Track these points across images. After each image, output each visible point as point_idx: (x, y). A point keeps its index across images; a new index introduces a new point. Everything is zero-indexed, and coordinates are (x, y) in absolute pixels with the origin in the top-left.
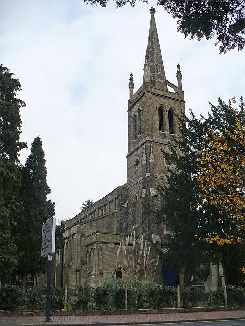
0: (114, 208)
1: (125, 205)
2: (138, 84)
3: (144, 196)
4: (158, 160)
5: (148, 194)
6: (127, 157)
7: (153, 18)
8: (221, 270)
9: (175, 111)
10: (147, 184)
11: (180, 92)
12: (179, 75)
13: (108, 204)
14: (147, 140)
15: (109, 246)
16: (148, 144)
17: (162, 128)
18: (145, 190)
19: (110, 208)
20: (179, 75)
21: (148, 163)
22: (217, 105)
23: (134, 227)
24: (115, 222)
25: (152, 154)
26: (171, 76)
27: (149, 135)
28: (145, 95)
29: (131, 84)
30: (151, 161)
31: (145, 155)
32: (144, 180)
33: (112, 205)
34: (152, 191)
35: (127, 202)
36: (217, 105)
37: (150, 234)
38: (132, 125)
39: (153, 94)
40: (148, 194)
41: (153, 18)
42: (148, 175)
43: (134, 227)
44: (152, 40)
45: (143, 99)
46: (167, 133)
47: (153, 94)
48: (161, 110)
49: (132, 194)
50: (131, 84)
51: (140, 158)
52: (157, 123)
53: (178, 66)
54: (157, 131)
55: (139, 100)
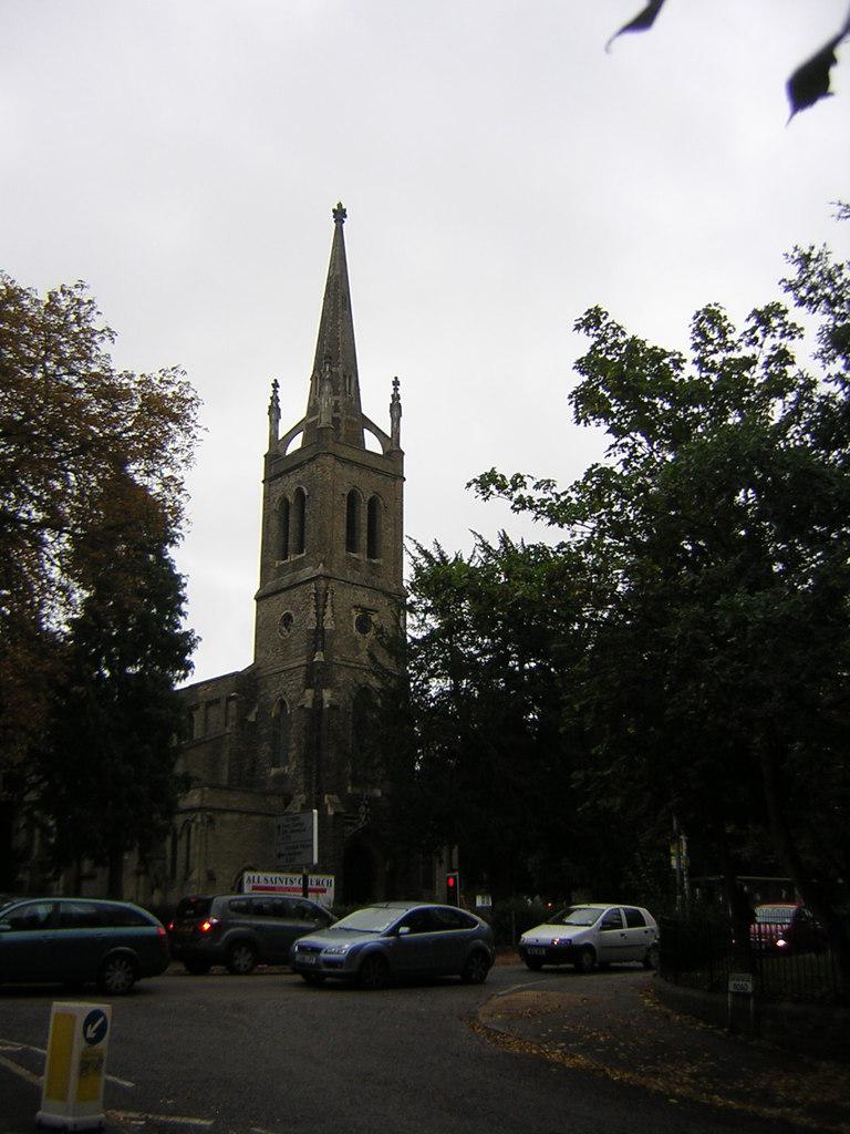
0: (222, 720)
1: (251, 718)
2: (295, 409)
3: (309, 705)
4: (341, 622)
5: (318, 701)
6: (259, 598)
7: (339, 233)
8: (455, 857)
9: (381, 502)
10: (316, 677)
11: (393, 453)
12: (396, 409)
13: (202, 708)
14: (320, 575)
15: (228, 817)
16: (323, 583)
17: (351, 545)
18: (309, 692)
19: (206, 720)
20: (396, 409)
21: (319, 632)
22: (496, 545)
23: (274, 771)
24: (225, 755)
25: (329, 610)
26: (374, 405)
27: (324, 562)
28: (320, 460)
29: (274, 411)
30: (328, 626)
31: (313, 610)
32: (311, 666)
33: (215, 713)
34: (327, 695)
35: (256, 710)
36: (496, 545)
37: (320, 793)
38: (274, 522)
39: (337, 458)
40: (318, 701)
41: (339, 233)
42: (319, 657)
43: (274, 771)
44: (335, 301)
45: (313, 467)
46: (361, 556)
47: (337, 458)
48: (352, 498)
49: (272, 692)
50: (274, 411)
51: (297, 611)
52: (343, 531)
53: (396, 383)
54: (342, 552)
55: (300, 465)
